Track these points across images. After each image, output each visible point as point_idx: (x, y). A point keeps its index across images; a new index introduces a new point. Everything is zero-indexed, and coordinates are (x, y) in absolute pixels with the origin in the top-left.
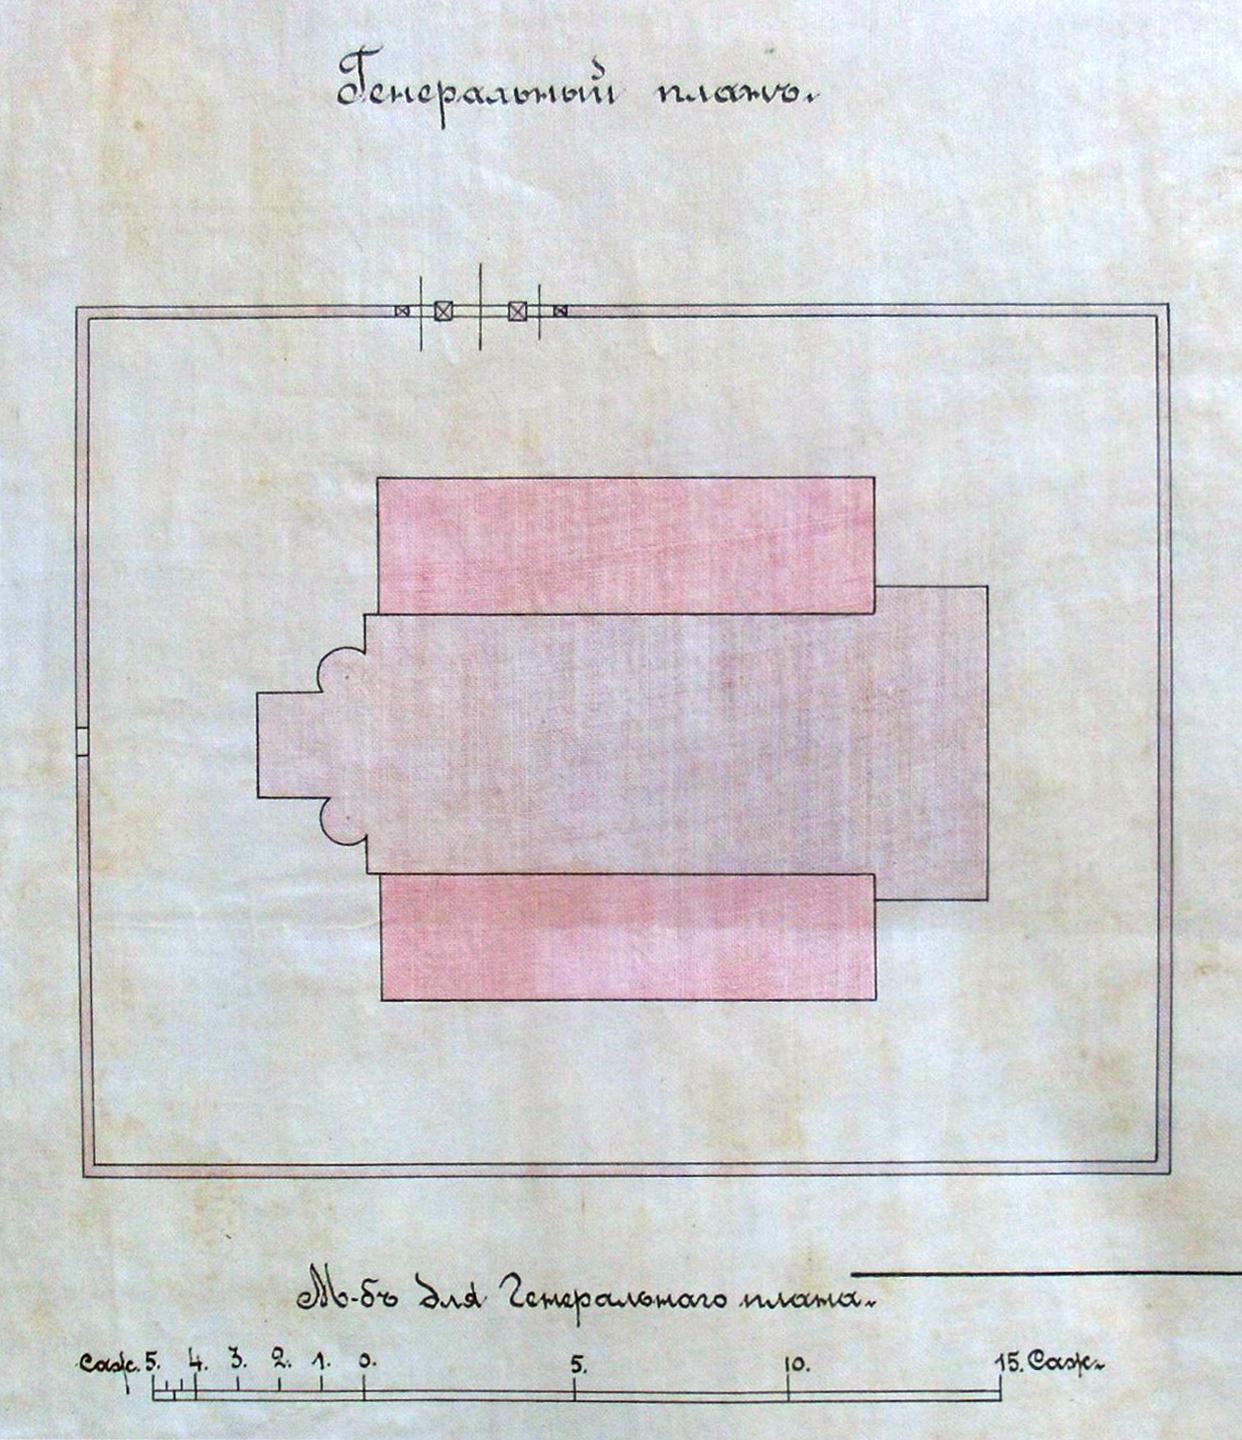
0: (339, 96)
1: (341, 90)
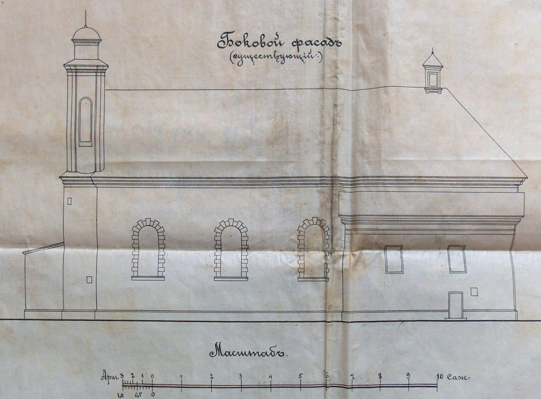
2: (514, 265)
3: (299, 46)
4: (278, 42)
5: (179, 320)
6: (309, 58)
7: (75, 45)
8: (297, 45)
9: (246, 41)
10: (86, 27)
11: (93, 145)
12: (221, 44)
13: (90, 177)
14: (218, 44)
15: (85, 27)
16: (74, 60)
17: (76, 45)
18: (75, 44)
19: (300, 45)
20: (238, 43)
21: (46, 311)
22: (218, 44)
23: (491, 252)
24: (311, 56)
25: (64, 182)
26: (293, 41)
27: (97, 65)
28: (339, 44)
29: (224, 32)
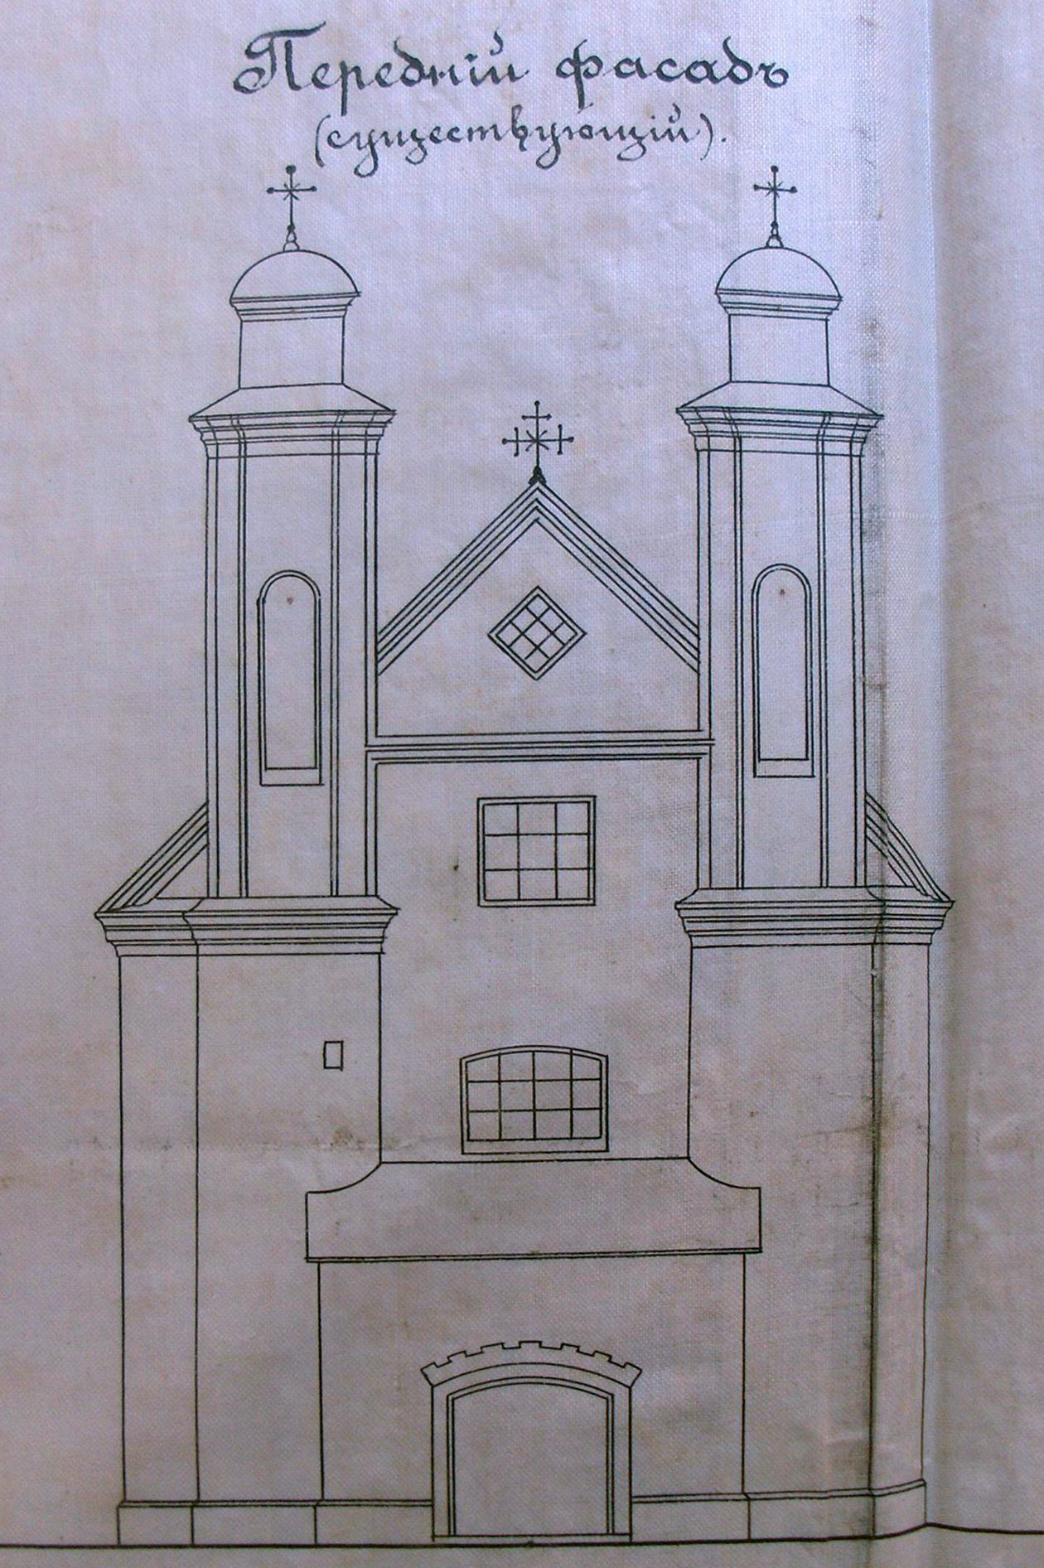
0: (644, 153)
1: (561, 65)
2: (857, 1534)
3: (586, 82)
4: (501, 71)
5: (1021, 1536)
6: (672, 139)
7: (242, 321)
8: (577, 73)
9: (518, 126)
10: (774, 242)
11: (817, 773)
12: (248, 81)
13: (184, 914)
14: (644, 153)
15: (767, 246)
16: (237, 391)
17: (246, 321)
18: (243, 318)
19: (588, 75)
20: (774, 73)
21: (451, 1437)
22: (369, 175)
23: (878, 1406)
24: (681, 132)
25: (112, 935)
26: (621, 59)
27: (824, 414)
28: (778, 79)
29: (245, 96)
